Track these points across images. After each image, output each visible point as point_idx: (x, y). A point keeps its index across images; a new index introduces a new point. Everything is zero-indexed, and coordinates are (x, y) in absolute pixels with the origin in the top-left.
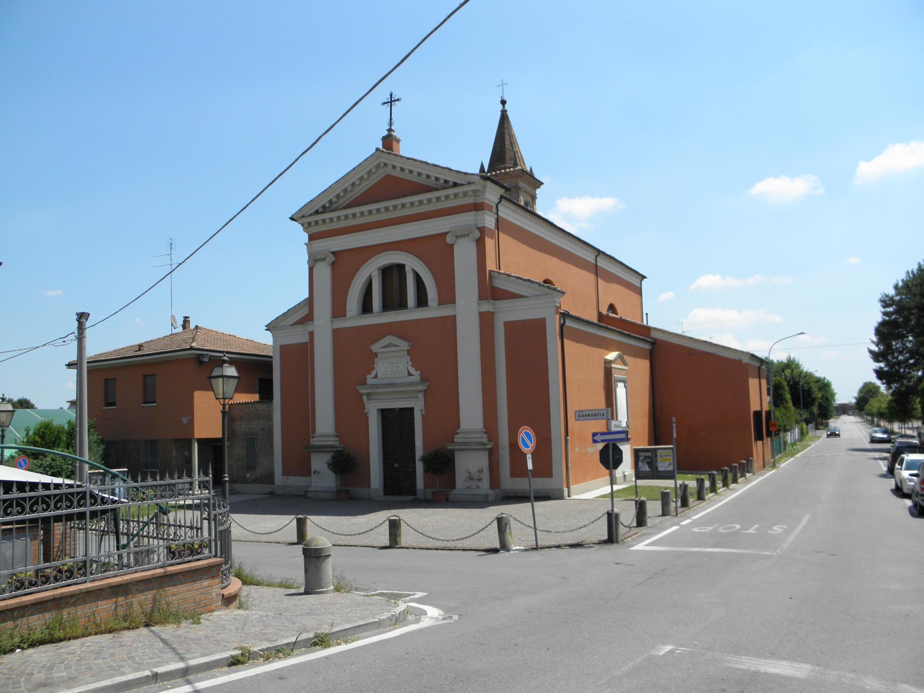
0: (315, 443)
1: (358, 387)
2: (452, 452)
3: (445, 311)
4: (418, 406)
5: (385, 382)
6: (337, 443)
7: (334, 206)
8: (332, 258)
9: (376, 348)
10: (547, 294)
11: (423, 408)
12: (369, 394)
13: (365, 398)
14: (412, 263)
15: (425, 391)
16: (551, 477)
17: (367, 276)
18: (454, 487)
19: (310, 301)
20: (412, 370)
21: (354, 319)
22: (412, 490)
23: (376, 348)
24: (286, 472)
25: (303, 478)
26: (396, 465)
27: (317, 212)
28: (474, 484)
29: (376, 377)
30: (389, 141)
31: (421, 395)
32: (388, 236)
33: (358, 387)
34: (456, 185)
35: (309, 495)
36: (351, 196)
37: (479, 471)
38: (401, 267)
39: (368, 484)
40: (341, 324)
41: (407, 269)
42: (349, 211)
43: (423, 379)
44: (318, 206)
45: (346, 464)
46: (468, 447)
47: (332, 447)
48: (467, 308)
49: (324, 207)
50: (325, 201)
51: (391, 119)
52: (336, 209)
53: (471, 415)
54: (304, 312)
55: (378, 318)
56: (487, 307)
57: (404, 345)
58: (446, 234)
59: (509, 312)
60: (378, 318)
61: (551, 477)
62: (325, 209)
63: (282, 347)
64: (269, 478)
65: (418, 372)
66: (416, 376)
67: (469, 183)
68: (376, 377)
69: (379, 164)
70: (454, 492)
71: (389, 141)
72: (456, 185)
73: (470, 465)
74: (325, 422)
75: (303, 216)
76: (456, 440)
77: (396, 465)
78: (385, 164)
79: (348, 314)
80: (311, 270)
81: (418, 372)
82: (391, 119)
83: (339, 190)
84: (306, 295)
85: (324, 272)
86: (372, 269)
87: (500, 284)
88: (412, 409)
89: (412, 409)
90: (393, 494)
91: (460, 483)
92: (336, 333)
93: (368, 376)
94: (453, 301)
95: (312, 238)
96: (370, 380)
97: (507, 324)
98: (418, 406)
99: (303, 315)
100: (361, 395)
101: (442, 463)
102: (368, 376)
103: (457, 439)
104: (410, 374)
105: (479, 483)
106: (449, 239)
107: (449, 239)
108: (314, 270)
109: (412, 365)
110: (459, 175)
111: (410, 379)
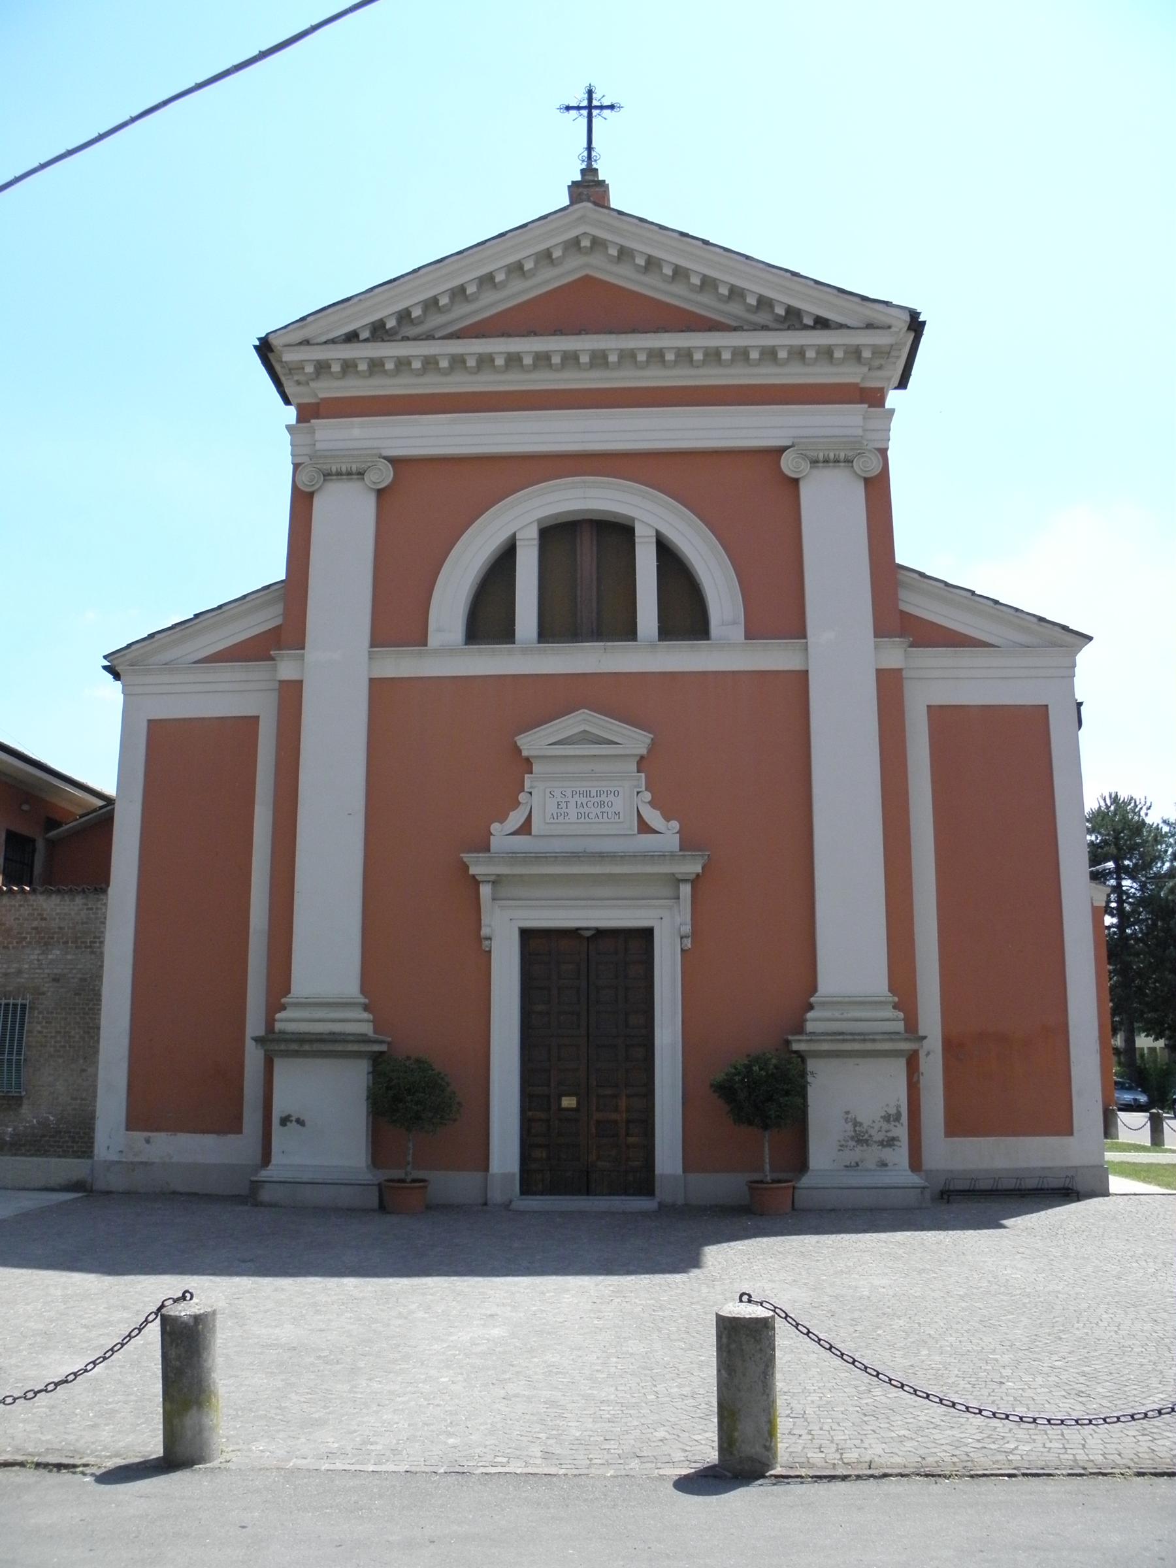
0: (291, 1027)
1: (467, 857)
2: (801, 1057)
3: (774, 657)
4: (670, 927)
5: (556, 846)
6: (367, 1029)
7: (435, 321)
8: (384, 476)
9: (531, 743)
10: (1054, 645)
11: (687, 929)
12: (496, 881)
13: (485, 890)
14: (653, 515)
15: (696, 881)
16: (1070, 1133)
17: (510, 533)
18: (802, 1166)
19: (293, 591)
20: (654, 818)
21: (445, 652)
22: (642, 1180)
23: (531, 743)
24: (141, 1117)
25: (209, 1140)
26: (568, 1102)
27: (352, 337)
28: (872, 1154)
29: (525, 828)
30: (589, 188)
31: (686, 890)
32: (584, 441)
33: (467, 857)
34: (822, 323)
35: (265, 1195)
36: (490, 304)
37: (887, 1118)
38: (616, 534)
39: (484, 1163)
40: (402, 665)
41: (639, 530)
42: (475, 347)
43: (688, 844)
44: (360, 322)
45: (412, 1100)
46: (856, 1047)
47: (363, 1039)
48: (840, 652)
49: (404, 316)
50: (386, 311)
51: (590, 148)
52: (429, 337)
53: (850, 957)
54: (267, 619)
55: (526, 657)
56: (895, 655)
57: (637, 741)
58: (781, 450)
59: (941, 682)
60: (526, 657)
61: (1070, 1133)
62: (379, 331)
63: (156, 728)
64: (76, 1136)
65: (675, 825)
66: (668, 835)
67: (870, 326)
68: (525, 828)
69: (576, 242)
70: (805, 1181)
71: (589, 188)
72: (822, 323)
73: (848, 1100)
74: (328, 960)
75: (306, 342)
76: (810, 1027)
77: (568, 1102)
78: (597, 243)
79: (434, 640)
80: (302, 503)
81: (675, 825)
82: (590, 148)
83: (440, 288)
84: (277, 572)
85: (349, 517)
86: (520, 517)
87: (914, 604)
88: (646, 935)
89: (646, 935)
90: (554, 1189)
91: (823, 1154)
92: (382, 692)
93: (495, 827)
94: (797, 630)
95: (307, 414)
96: (501, 835)
97: (935, 712)
98: (670, 927)
99: (273, 626)
100: (475, 882)
101: (762, 1098)
102: (495, 827)
103: (815, 1021)
104: (644, 827)
105: (887, 1154)
106: (788, 464)
107: (788, 464)
108: (320, 505)
109: (653, 804)
110: (841, 301)
111: (647, 842)
